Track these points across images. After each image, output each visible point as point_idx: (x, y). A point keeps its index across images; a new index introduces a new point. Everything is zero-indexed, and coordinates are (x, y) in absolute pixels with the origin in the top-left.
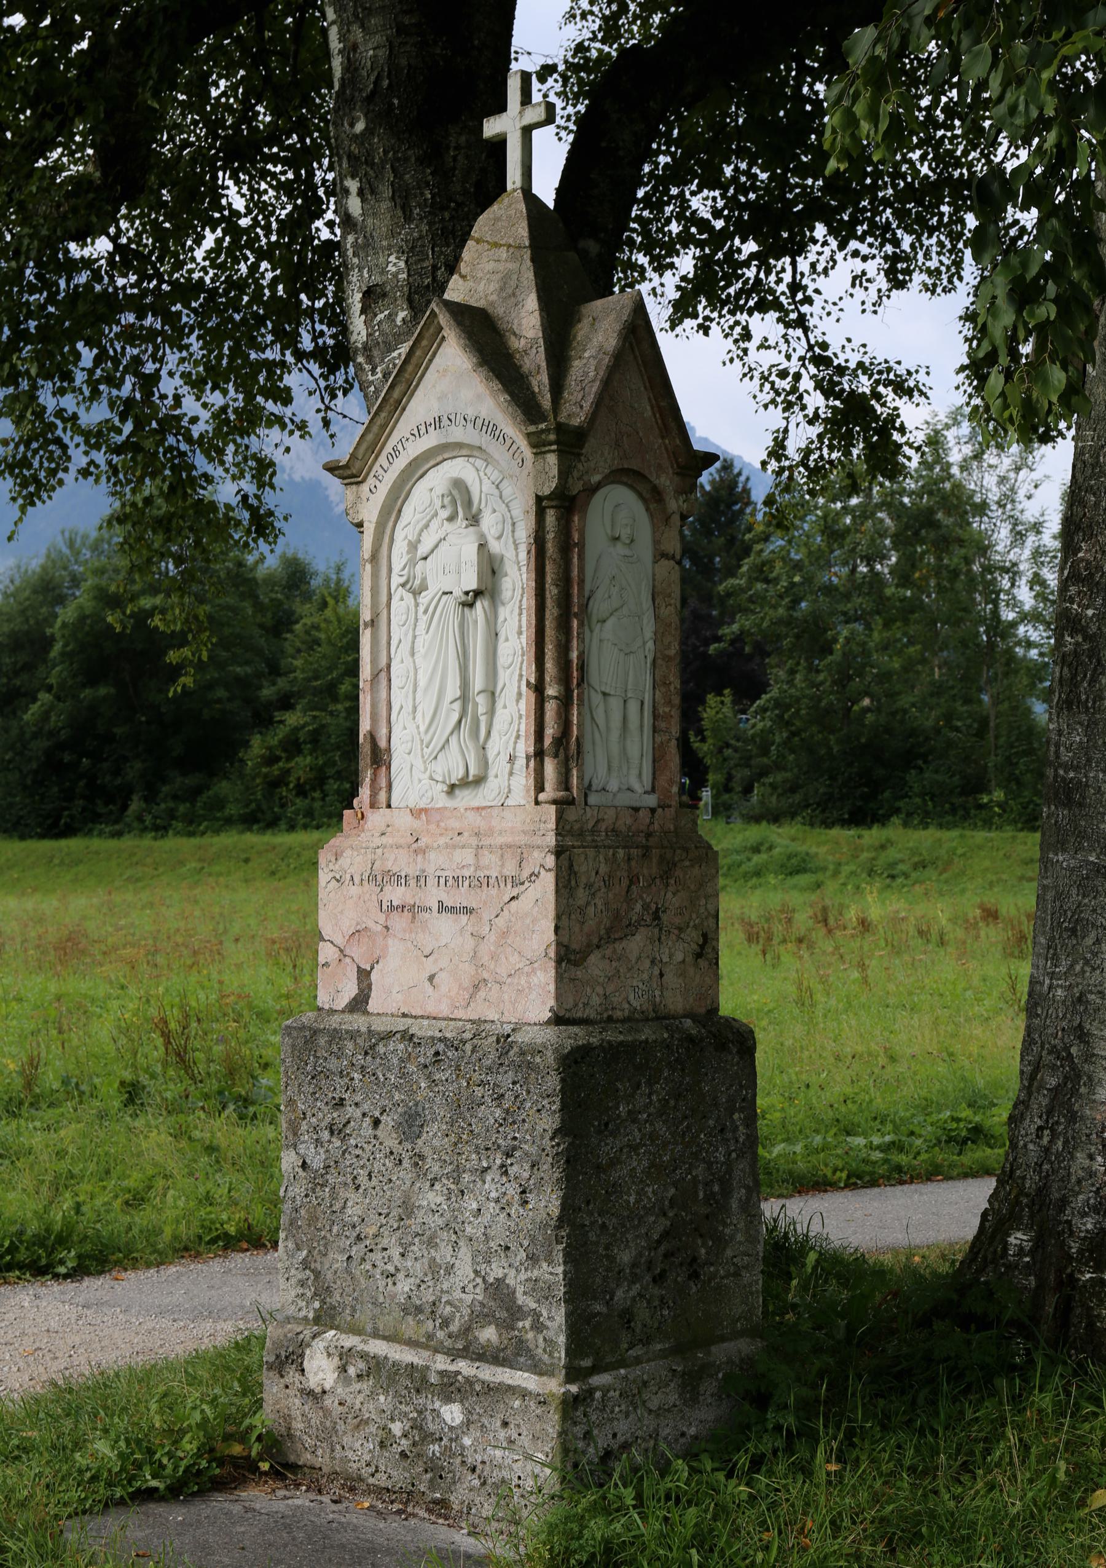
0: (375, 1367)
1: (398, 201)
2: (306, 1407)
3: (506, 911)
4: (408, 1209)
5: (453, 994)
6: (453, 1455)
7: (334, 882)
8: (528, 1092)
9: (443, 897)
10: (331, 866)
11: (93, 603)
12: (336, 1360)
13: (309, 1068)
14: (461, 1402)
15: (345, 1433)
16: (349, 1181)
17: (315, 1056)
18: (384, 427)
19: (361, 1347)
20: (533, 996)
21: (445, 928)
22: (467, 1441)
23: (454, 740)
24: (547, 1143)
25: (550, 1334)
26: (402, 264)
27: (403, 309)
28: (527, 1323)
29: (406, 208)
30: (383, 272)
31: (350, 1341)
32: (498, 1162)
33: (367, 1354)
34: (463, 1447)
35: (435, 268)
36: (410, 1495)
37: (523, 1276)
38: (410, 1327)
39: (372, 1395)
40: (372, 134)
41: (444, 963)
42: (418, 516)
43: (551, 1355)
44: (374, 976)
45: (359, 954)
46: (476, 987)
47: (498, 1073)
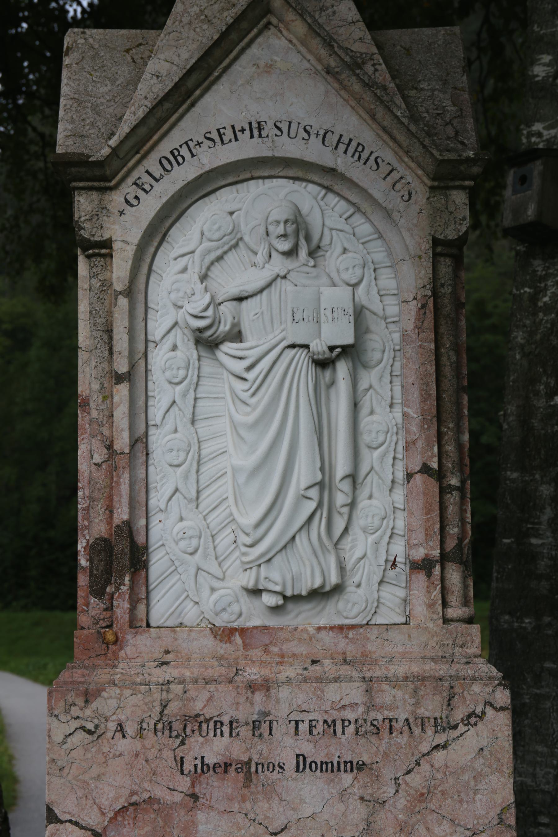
3: (425, 766)
7: (81, 736)
9: (306, 748)
10: (75, 712)
11: (287, 242)
18: (163, 121)
23: (301, 542)
42: (206, 245)
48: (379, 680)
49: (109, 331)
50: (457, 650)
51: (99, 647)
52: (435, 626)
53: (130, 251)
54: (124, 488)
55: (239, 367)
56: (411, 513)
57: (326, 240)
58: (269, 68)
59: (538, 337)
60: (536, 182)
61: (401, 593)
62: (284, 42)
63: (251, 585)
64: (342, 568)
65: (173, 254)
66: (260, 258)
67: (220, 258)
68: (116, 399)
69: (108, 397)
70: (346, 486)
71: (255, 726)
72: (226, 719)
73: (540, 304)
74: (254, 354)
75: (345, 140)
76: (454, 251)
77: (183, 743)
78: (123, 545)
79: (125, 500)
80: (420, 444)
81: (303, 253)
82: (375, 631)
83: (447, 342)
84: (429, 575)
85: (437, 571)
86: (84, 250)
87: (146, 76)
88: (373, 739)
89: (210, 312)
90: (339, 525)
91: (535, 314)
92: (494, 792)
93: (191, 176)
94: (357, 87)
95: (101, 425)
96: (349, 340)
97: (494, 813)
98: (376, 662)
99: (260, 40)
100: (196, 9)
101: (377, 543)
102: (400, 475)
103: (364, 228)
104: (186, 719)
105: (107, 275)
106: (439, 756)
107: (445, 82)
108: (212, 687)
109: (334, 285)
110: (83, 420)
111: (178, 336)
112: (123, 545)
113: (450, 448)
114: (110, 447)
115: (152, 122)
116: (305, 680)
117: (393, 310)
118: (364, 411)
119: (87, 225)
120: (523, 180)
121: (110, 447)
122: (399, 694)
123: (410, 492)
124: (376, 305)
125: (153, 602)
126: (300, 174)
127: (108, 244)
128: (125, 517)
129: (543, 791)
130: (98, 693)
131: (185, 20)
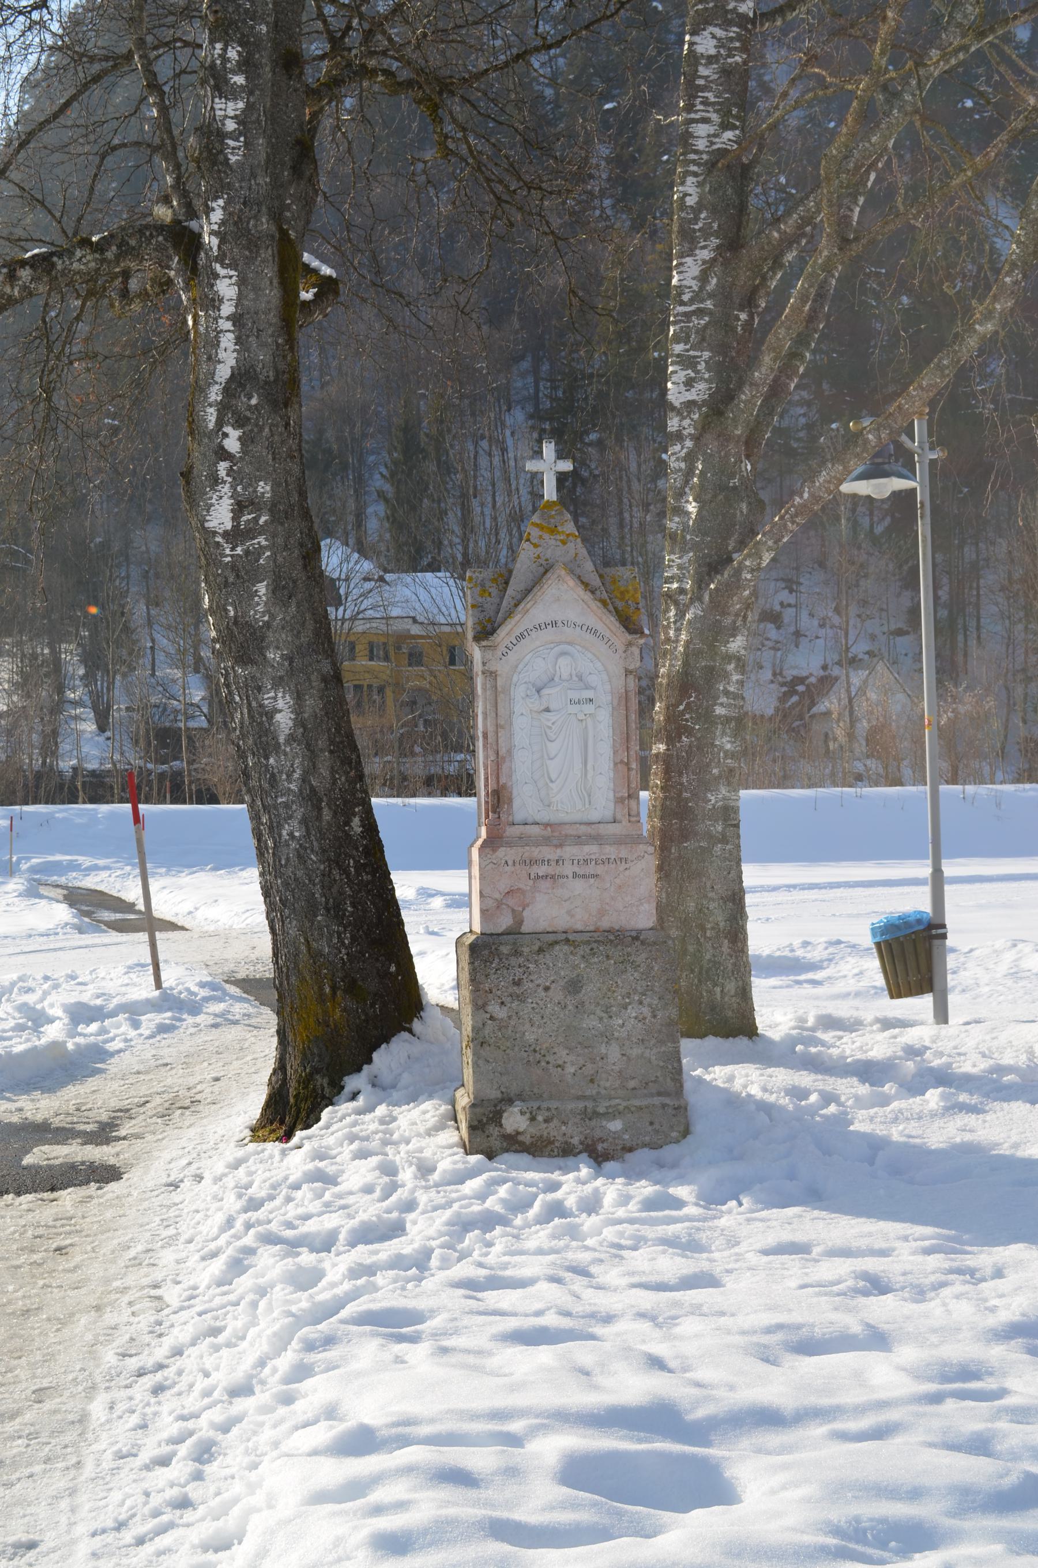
21: (578, 886)
26: (268, 488)
37: (655, 1051)
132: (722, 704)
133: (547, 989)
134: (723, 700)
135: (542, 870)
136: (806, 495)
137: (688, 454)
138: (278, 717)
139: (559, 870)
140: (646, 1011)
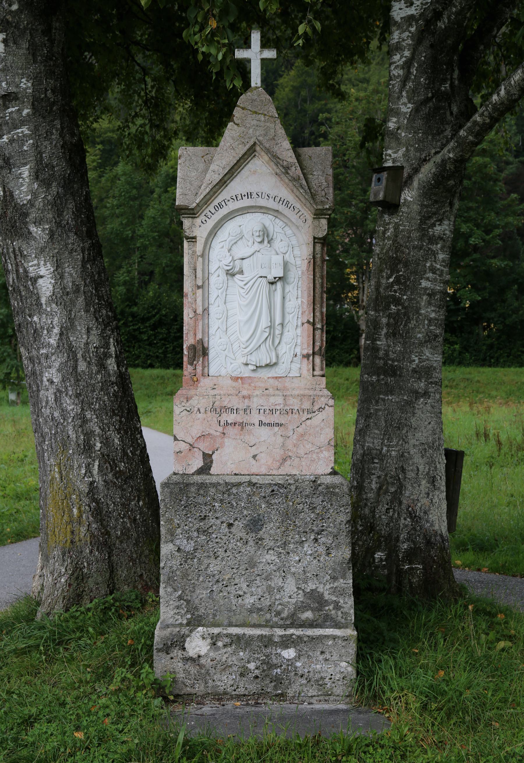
0: (237, 640)
1: (31, 51)
2: (187, 666)
3: (303, 425)
4: (252, 564)
5: (269, 463)
6: (289, 672)
7: (185, 412)
8: (331, 505)
10: (183, 404)
12: (209, 641)
13: (182, 503)
14: (295, 647)
15: (215, 674)
16: (212, 554)
17: (187, 497)
18: (215, 192)
19: (225, 632)
20: (321, 462)
21: (264, 433)
22: (298, 664)
23: (263, 347)
24: (343, 526)
25: (346, 610)
26: (29, 85)
27: (27, 108)
28: (331, 607)
29: (34, 55)
30: (18, 86)
31: (216, 631)
32: (312, 537)
33: (231, 635)
34: (296, 667)
35: (46, 90)
36: (262, 694)
37: (328, 586)
38: (254, 618)
39: (234, 653)
40: (22, 12)
41: (263, 448)
42: (231, 238)
43: (346, 619)
44: (214, 457)
45: (205, 446)
46: (284, 460)
47: (312, 497)
48: (289, 396)
49: (195, 270)
50: (317, 386)
51: (191, 383)
52: (310, 377)
53: (203, 240)
54: (200, 327)
55: (242, 284)
56: (303, 337)
57: (275, 237)
58: (255, 172)
59: (385, 251)
60: (384, 182)
61: (299, 366)
62: (261, 162)
63: (245, 362)
64: (277, 357)
65: (219, 241)
66: (250, 244)
67: (236, 243)
68: (197, 295)
69: (195, 294)
70: (279, 327)
71: (245, 410)
72: (235, 408)
73: (386, 236)
74: (248, 279)
75: (282, 200)
76: (322, 241)
77: (220, 416)
78: (200, 347)
79: (201, 331)
80: (307, 312)
81: (266, 241)
82: (288, 379)
83: (318, 275)
84: (308, 359)
85: (311, 358)
86: (187, 239)
87: (210, 171)
88: (286, 416)
89: (231, 264)
90: (277, 341)
91: (384, 240)
92: (327, 434)
93: (225, 213)
94: (287, 181)
95: (192, 304)
96: (281, 275)
97: (327, 441)
98: (288, 390)
99: (252, 161)
100: (229, 144)
101: (290, 348)
102: (300, 324)
103: (289, 232)
104: (221, 408)
105: (194, 249)
106: (308, 422)
107: (323, 172)
108: (230, 397)
109: (278, 254)
110: (185, 301)
111: (220, 271)
112: (200, 347)
113: (318, 314)
114: (195, 312)
115: (211, 193)
116: (263, 395)
117: (299, 262)
118: (287, 300)
119: (187, 231)
120: (379, 180)
121: (195, 312)
122: (295, 401)
123: (303, 330)
124: (292, 261)
125: (210, 367)
126: (266, 211)
127: (195, 238)
128: (201, 337)
129: (376, 449)
130: (191, 398)
131: (225, 148)
132: (428, 279)
133: (230, 525)
134: (430, 275)
135: (231, 418)
136: (503, 92)
137: (405, 63)
138: (40, 281)
139: (246, 419)
140: (321, 549)
